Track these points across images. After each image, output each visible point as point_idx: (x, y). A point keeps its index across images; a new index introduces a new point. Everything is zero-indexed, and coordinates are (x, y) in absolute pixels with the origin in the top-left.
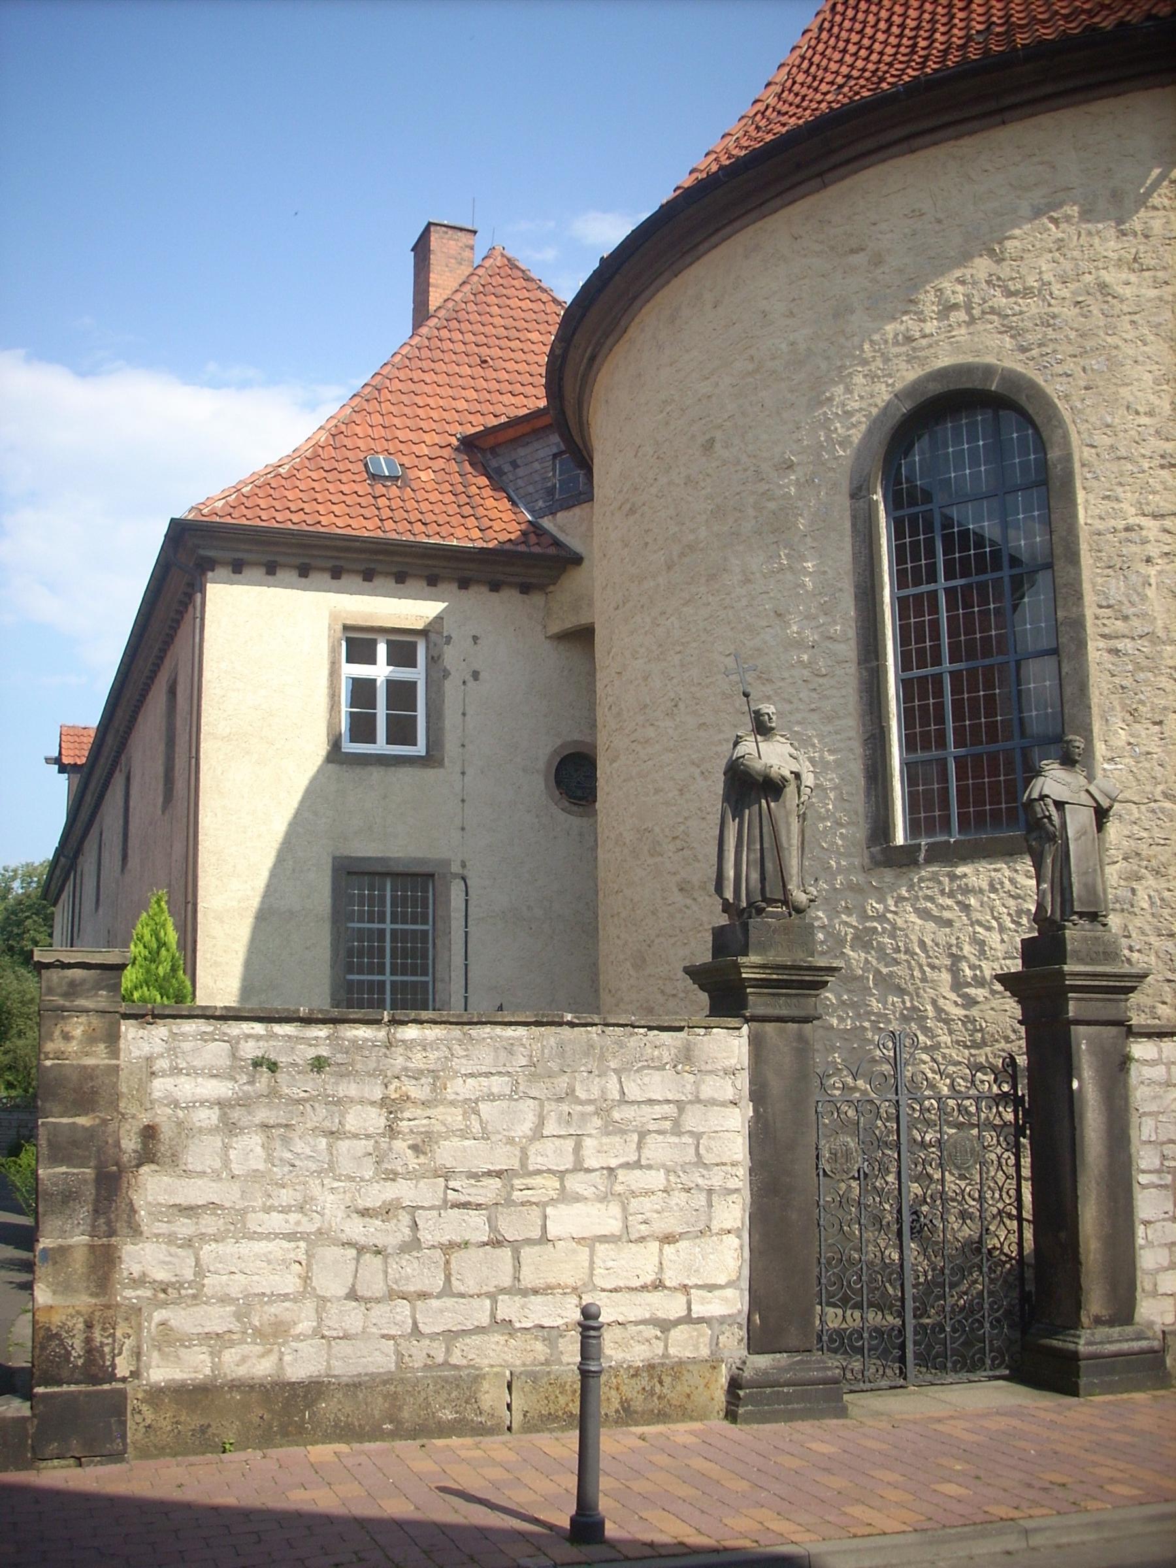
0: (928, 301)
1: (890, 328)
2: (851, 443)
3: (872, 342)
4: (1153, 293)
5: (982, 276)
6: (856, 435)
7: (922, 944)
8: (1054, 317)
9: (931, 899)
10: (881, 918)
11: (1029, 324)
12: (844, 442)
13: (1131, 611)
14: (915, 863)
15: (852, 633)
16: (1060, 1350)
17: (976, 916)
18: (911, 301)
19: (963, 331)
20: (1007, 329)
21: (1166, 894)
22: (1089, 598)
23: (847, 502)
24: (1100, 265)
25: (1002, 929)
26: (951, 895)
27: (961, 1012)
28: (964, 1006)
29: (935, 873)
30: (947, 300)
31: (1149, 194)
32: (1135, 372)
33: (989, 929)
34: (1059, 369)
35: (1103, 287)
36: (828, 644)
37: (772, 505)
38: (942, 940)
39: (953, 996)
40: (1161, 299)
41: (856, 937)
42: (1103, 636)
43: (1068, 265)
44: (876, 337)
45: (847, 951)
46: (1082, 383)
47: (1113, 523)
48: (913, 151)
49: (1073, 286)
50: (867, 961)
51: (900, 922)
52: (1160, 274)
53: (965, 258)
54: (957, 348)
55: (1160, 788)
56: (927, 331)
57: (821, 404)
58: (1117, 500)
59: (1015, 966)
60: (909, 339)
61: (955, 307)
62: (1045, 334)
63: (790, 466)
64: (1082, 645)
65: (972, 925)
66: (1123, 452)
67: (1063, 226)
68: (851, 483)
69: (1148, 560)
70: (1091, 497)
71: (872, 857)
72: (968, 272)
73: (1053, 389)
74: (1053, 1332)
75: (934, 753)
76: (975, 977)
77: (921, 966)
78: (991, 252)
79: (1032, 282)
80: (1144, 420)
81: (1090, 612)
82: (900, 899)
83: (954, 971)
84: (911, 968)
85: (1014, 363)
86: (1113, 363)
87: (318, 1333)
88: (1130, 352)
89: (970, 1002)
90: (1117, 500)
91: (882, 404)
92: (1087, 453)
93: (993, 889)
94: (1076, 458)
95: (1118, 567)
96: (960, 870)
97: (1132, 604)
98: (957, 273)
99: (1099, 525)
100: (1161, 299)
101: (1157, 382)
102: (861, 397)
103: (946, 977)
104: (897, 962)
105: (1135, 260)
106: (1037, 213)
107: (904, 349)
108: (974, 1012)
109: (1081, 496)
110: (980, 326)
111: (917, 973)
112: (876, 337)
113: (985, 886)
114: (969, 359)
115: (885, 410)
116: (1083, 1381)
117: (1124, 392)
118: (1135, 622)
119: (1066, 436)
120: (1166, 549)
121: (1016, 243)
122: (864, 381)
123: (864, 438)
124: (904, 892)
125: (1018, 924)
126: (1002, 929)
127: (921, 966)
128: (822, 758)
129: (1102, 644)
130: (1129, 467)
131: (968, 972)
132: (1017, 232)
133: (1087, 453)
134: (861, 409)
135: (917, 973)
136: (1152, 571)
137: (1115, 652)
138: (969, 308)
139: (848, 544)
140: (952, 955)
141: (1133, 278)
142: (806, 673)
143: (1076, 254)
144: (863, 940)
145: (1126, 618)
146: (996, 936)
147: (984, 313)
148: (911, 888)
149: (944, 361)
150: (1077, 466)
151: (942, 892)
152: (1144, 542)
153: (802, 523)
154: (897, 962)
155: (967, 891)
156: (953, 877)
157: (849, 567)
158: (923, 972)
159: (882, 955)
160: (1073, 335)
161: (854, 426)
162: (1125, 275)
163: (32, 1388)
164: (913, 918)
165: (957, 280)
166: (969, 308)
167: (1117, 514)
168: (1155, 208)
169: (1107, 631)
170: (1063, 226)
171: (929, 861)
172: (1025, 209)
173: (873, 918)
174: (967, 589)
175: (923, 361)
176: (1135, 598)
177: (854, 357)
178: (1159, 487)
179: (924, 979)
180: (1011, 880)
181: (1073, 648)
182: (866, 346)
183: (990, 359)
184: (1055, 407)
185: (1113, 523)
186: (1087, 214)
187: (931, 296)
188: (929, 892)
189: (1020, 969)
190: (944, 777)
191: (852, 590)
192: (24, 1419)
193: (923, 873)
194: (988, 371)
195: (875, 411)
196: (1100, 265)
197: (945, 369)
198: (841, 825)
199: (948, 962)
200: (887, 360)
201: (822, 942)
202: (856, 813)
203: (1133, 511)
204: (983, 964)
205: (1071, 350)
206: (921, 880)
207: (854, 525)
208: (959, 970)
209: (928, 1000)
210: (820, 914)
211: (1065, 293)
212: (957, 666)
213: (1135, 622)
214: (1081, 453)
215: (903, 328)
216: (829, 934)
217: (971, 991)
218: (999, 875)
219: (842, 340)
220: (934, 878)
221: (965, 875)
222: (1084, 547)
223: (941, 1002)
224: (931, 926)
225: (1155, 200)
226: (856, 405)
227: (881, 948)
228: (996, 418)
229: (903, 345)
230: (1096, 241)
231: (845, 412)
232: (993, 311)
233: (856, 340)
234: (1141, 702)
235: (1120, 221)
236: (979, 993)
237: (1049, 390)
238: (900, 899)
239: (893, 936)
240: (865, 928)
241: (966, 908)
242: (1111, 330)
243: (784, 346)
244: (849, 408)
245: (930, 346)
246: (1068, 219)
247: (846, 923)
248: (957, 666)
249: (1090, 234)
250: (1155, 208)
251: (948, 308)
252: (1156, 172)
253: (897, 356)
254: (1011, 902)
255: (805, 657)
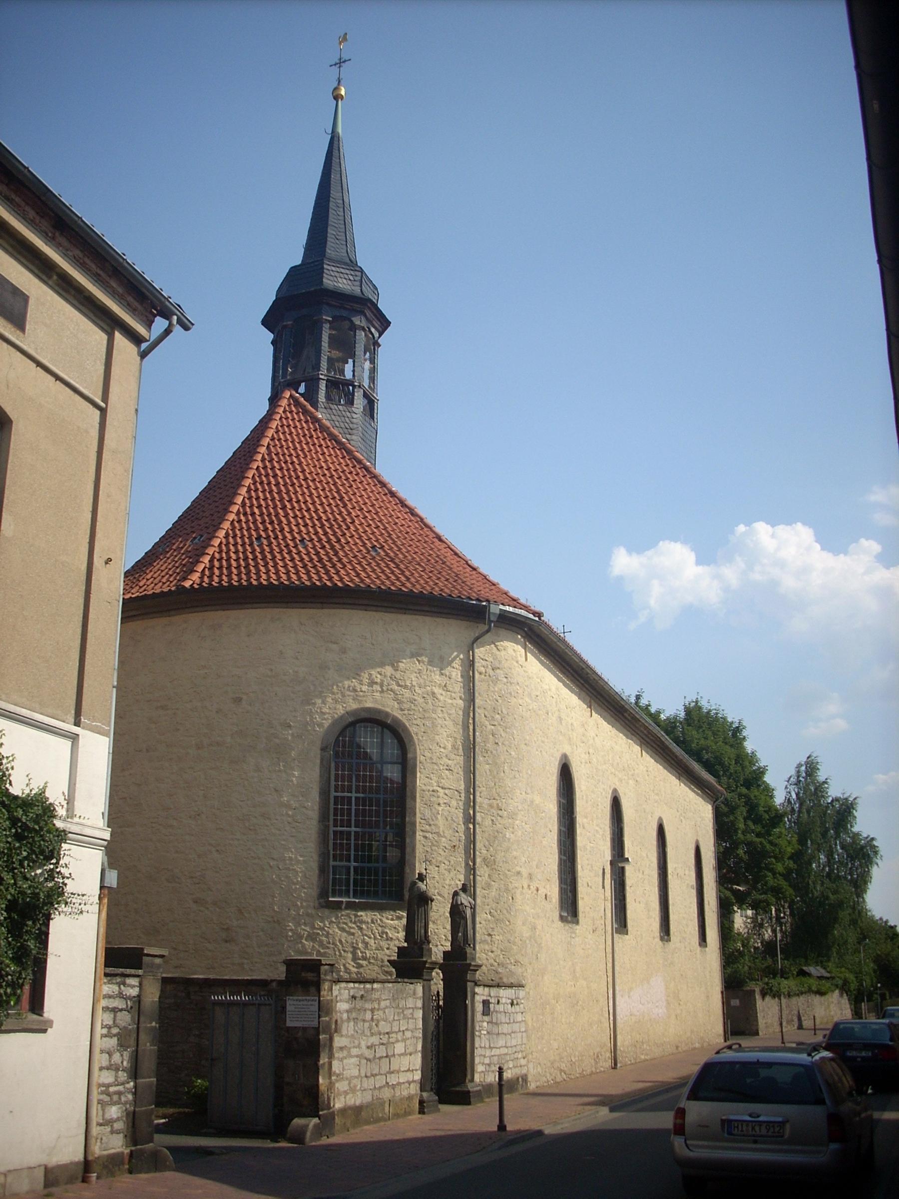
0: (365, 677)
1: (347, 683)
2: (323, 727)
3: (337, 686)
4: (450, 701)
5: (389, 674)
6: (326, 724)
7: (340, 941)
8: (415, 700)
9: (346, 924)
10: (322, 929)
11: (405, 700)
12: (320, 725)
13: (432, 823)
14: (340, 908)
15: (316, 807)
16: (459, 1091)
17: (365, 932)
18: (357, 674)
19: (378, 694)
20: (396, 700)
21: (436, 930)
22: (418, 815)
23: (319, 752)
24: (433, 684)
25: (375, 938)
26: (355, 923)
27: (356, 970)
28: (357, 968)
29: (349, 914)
30: (373, 679)
31: (452, 661)
32: (441, 731)
33: (370, 938)
34: (415, 722)
35: (433, 693)
36: (304, 810)
37: (277, 741)
38: (350, 941)
39: (353, 963)
40: (452, 704)
41: (308, 936)
42: (422, 831)
43: (422, 681)
44: (340, 685)
45: (304, 941)
46: (423, 730)
47: (428, 788)
48: (366, 610)
49: (423, 690)
50: (313, 946)
51: (331, 932)
52: (453, 694)
53: (382, 665)
54: (376, 701)
55: (436, 891)
56: (363, 690)
57: (309, 704)
58: (431, 779)
59: (394, 957)
60: (355, 690)
61: (376, 683)
62: (411, 707)
63: (290, 726)
64: (414, 833)
65: (363, 935)
66: (434, 761)
67: (421, 664)
68: (322, 743)
69: (439, 804)
70: (422, 776)
71: (320, 903)
72: (383, 670)
73: (413, 729)
74: (458, 1084)
75: (345, 863)
76: (362, 956)
77: (339, 950)
78: (393, 666)
79: (408, 684)
80: (442, 750)
81: (418, 820)
82: (331, 922)
83: (354, 953)
84: (334, 950)
85: (397, 714)
86: (434, 725)
87: (360, 1090)
88: (440, 722)
89: (360, 966)
90: (431, 779)
91: (340, 714)
92: (422, 758)
93: (373, 922)
94: (418, 759)
95: (430, 806)
96: (359, 914)
97: (433, 820)
98: (379, 670)
99: (424, 788)
100: (452, 704)
101: (448, 736)
102: (330, 708)
103: (350, 955)
104: (328, 948)
105: (445, 686)
106: (412, 656)
107: (352, 694)
108: (361, 970)
109: (418, 775)
110: (385, 695)
111: (337, 953)
112: (340, 685)
113: (370, 921)
114: (380, 707)
115: (342, 717)
116: (472, 1100)
117: (437, 737)
118: (433, 827)
119: (415, 750)
120: (445, 801)
121: (403, 665)
122: (331, 701)
123: (329, 726)
124: (333, 919)
125: (382, 937)
126: (375, 938)
127: (339, 950)
128: (296, 858)
129: (421, 833)
130: (436, 767)
131: (360, 954)
132: (404, 661)
133: (422, 758)
134: (329, 713)
135: (337, 953)
136: (440, 809)
137: (425, 837)
138: (382, 686)
139: (317, 769)
140: (353, 947)
141: (444, 693)
142: (290, 819)
143: (425, 677)
144: (312, 937)
145: (430, 825)
146: (373, 941)
147: (388, 689)
148: (337, 918)
149: (369, 705)
150: (418, 762)
151: (351, 921)
152: (438, 797)
153: (293, 754)
154: (328, 948)
155: (362, 922)
156: (356, 916)
157: (318, 779)
158: (340, 953)
159: (321, 944)
160: (421, 710)
161: (325, 719)
162: (441, 691)
163: (318, 1112)
164: (337, 930)
165: (378, 672)
166: (382, 686)
167: (431, 785)
168: (454, 668)
169: (423, 829)
170: (421, 664)
171: (346, 908)
172: (408, 653)
173: (318, 929)
174: (364, 799)
175: (360, 702)
176: (434, 818)
177: (328, 690)
178: (445, 777)
179: (340, 955)
180: (380, 920)
181: (411, 833)
182: (335, 687)
183: (388, 710)
184: (412, 736)
185: (428, 788)
186: (430, 663)
187: (366, 676)
188: (345, 921)
189: (396, 958)
190: (348, 873)
191: (318, 790)
192: (319, 1124)
193: (343, 913)
194: (387, 714)
195: (336, 716)
196: (433, 684)
197: (370, 708)
198: (305, 888)
199: (351, 950)
200: (344, 696)
201: (291, 937)
202: (313, 884)
203: (435, 784)
204: (367, 951)
205: (420, 715)
206: (342, 915)
207: (322, 762)
208: (356, 953)
209: (341, 964)
210: (290, 924)
211: (419, 692)
212: (358, 829)
213: (433, 827)
214: (420, 758)
215: (352, 685)
216: (294, 933)
217: (360, 962)
218: (375, 917)
219: (322, 679)
220: (348, 915)
221: (361, 916)
222: (418, 795)
223: (347, 965)
224: (345, 934)
225: (454, 665)
226: (328, 711)
227: (321, 942)
228: (382, 732)
229: (351, 692)
230: (433, 674)
231: (321, 712)
232: (391, 690)
233: (330, 682)
234: (433, 858)
235: (441, 669)
236: (364, 963)
237: (411, 729)
238: (331, 922)
239: (327, 936)
240: (314, 933)
241: (361, 929)
242: (434, 711)
243: (291, 671)
244: (323, 711)
245: (364, 696)
246: (423, 662)
247: (304, 930)
248: (358, 829)
249: (431, 671)
250: (454, 668)
251: (372, 683)
252: (455, 653)
253: (349, 696)
254: (380, 928)
255: (290, 813)
